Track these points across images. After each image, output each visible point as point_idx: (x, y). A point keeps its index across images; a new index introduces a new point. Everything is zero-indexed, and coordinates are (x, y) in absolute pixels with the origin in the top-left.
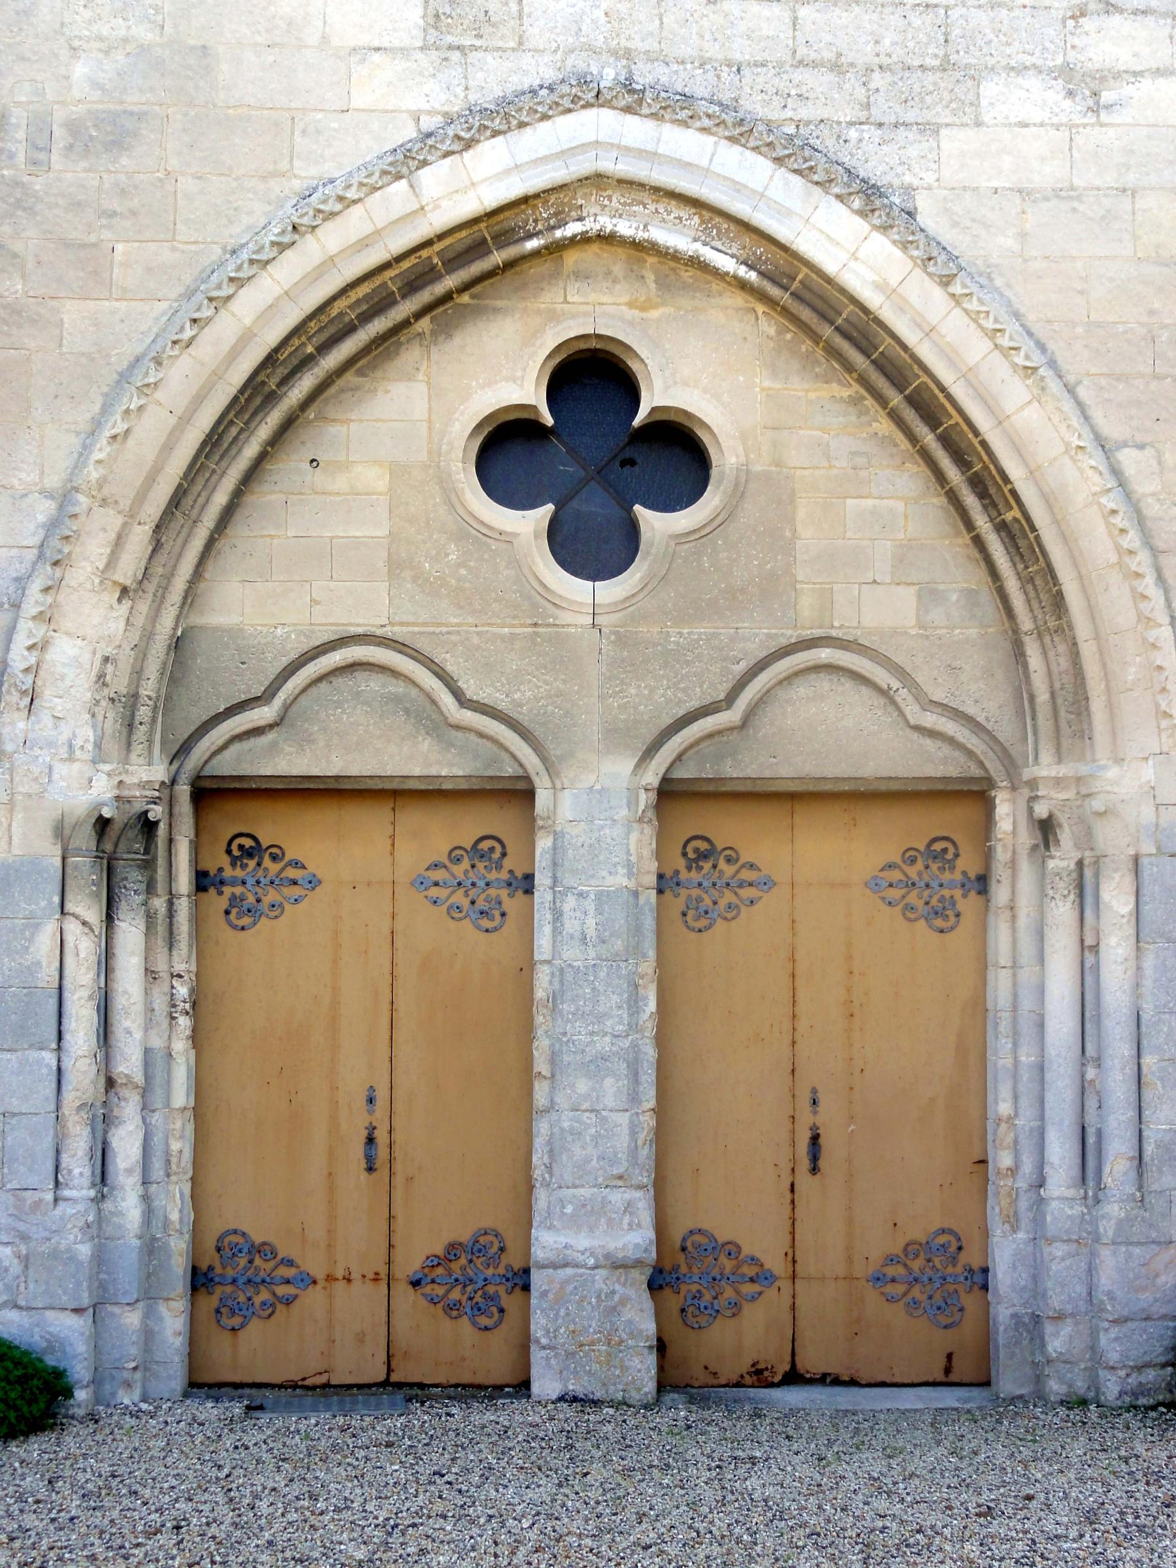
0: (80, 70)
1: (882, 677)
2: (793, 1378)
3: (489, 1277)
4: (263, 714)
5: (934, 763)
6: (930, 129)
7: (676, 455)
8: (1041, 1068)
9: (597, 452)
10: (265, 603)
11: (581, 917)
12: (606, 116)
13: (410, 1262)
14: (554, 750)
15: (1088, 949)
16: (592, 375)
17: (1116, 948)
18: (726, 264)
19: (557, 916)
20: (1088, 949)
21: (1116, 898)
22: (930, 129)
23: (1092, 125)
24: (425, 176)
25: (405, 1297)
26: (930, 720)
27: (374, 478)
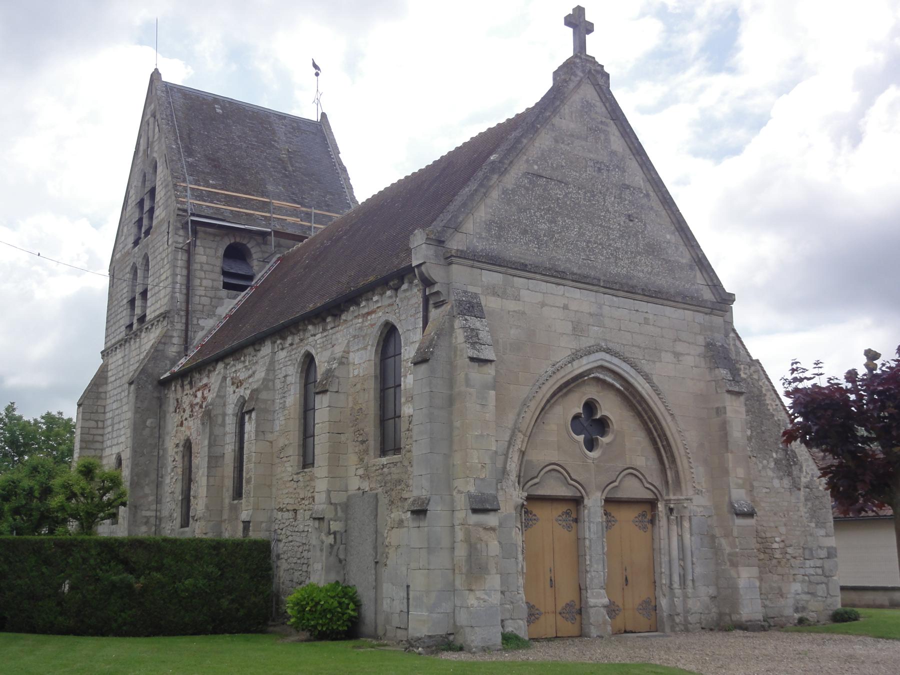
0: (512, 332)
1: (641, 476)
2: (626, 632)
3: (578, 610)
4: (536, 480)
5: (648, 495)
6: (654, 362)
7: (603, 425)
8: (670, 561)
9: (592, 425)
10: (541, 456)
11: (594, 527)
12: (603, 353)
13: (559, 609)
14: (588, 490)
15: (681, 537)
16: (590, 406)
17: (687, 536)
18: (618, 386)
19: (589, 528)
20: (681, 537)
21: (686, 524)
22: (654, 362)
23: (610, 341)
24: (574, 363)
25: (559, 617)
26: (648, 486)
27: (554, 427)
